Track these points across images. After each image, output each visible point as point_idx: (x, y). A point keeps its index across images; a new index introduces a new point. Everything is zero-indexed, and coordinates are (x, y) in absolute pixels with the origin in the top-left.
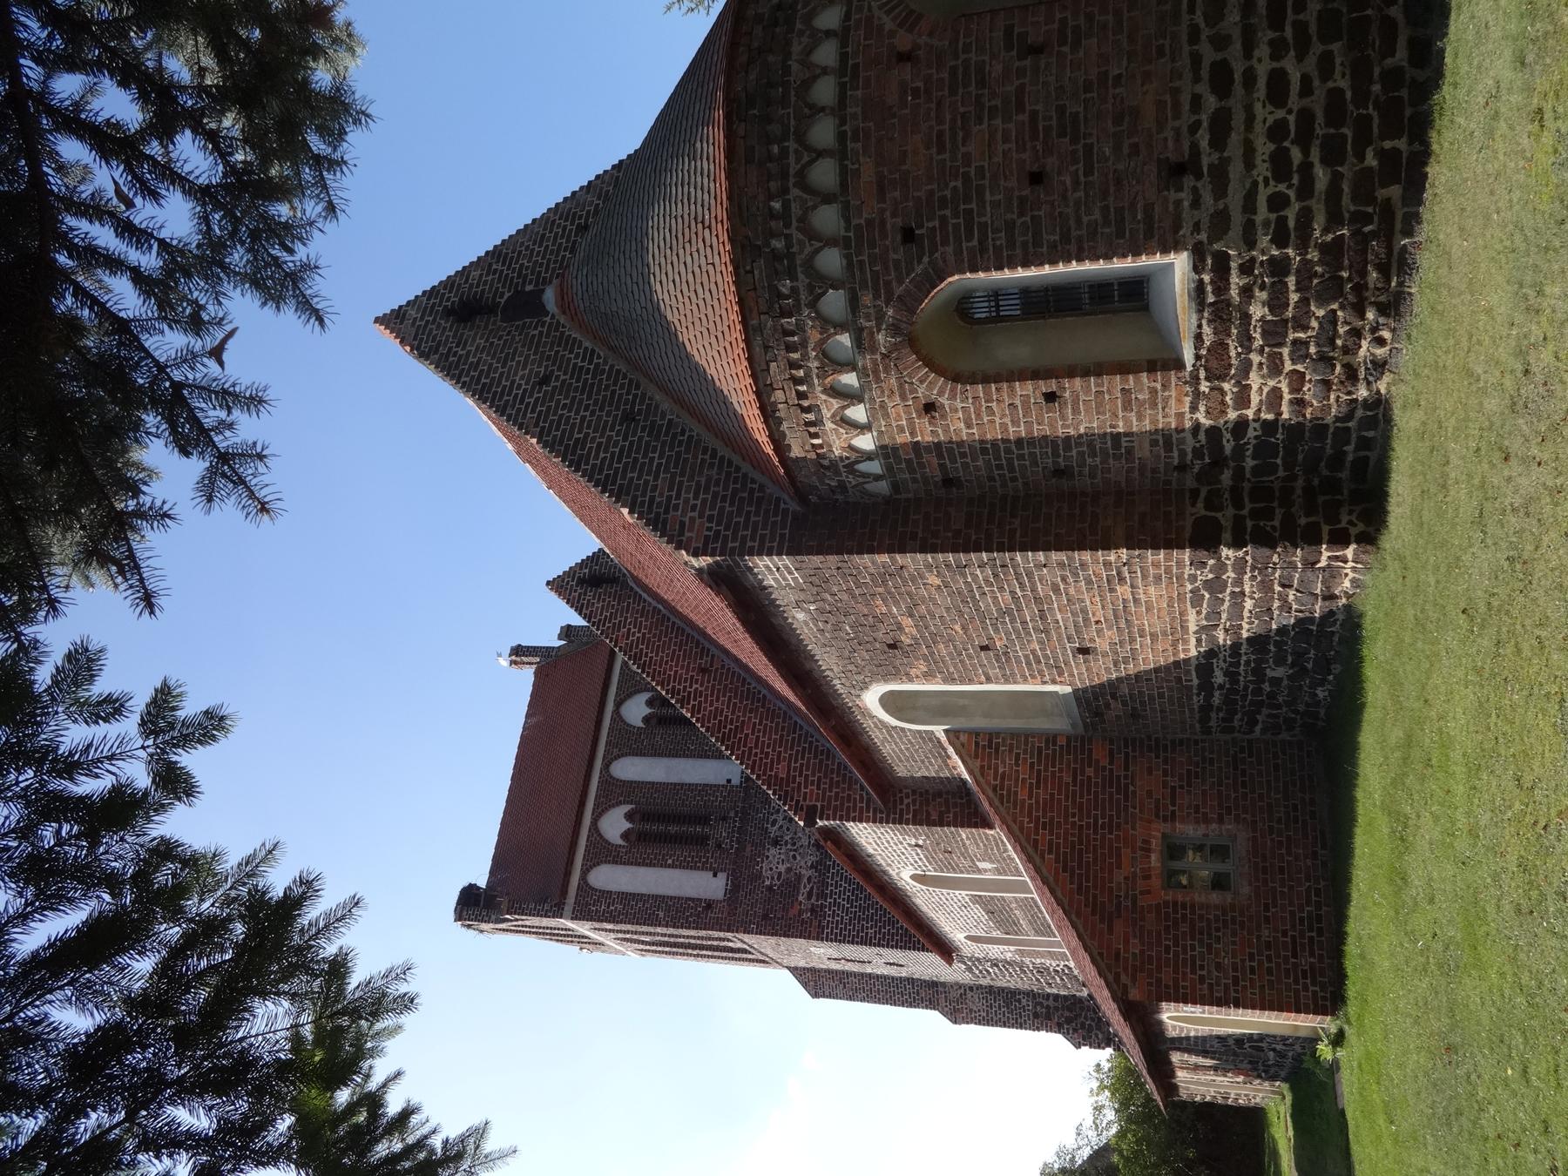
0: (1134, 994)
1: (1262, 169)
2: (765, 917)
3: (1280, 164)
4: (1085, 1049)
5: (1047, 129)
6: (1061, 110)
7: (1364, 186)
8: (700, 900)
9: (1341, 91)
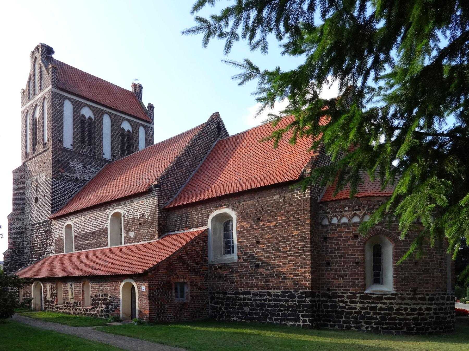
0: (150, 274)
1: (413, 307)
2: (59, 161)
3: (413, 310)
4: (3, 256)
5: (426, 266)
6: (429, 269)
7: (407, 325)
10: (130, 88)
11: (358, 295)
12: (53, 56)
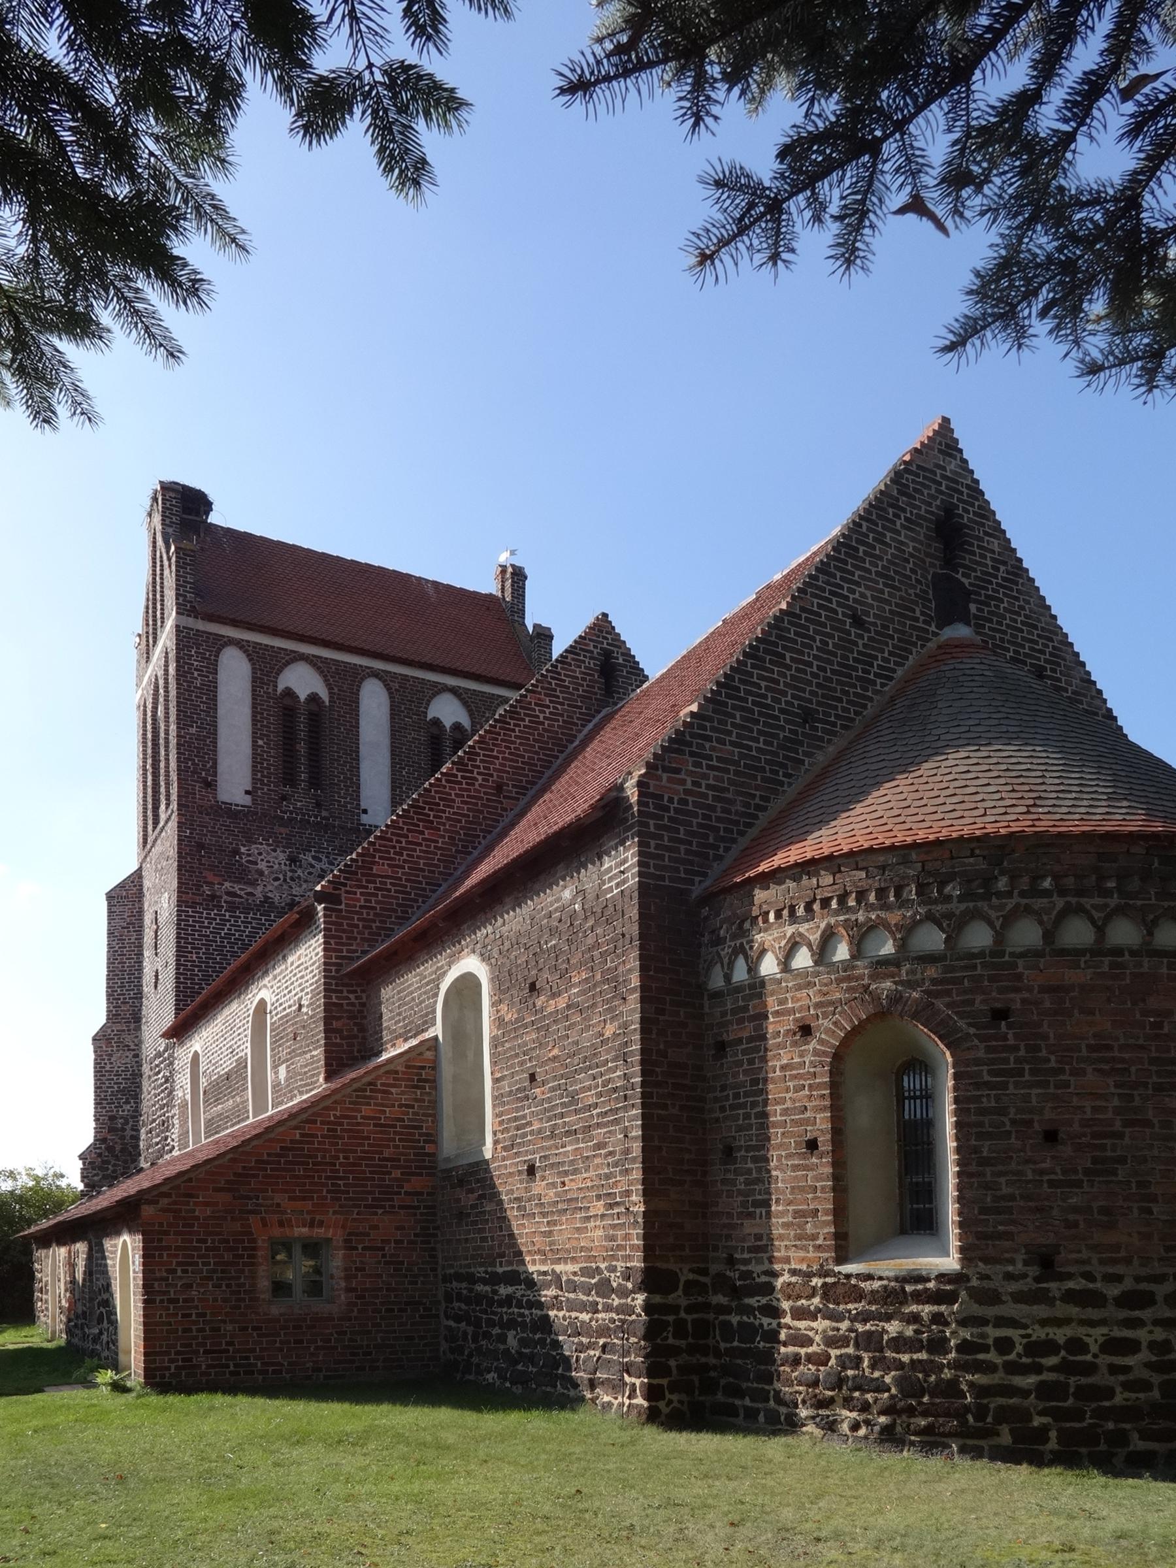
1: (1039, 1333)
2: (201, 846)
3: (1036, 1348)
4: (80, 1164)
5: (1103, 1147)
6: (1122, 1160)
10: (488, 585)
11: (816, 1282)
12: (214, 518)
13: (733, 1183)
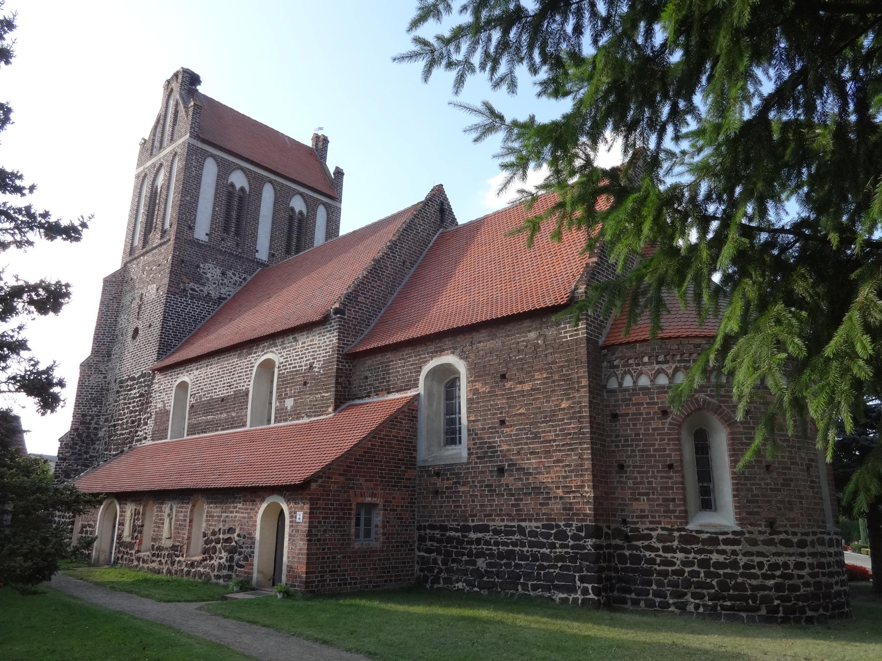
0: (314, 486)
1: (773, 560)
2: (183, 261)
3: (774, 566)
4: (58, 444)
5: (785, 474)
8: (194, 223)
9: (799, 590)
10: (309, 143)
11: (676, 534)
13: (626, 483)
